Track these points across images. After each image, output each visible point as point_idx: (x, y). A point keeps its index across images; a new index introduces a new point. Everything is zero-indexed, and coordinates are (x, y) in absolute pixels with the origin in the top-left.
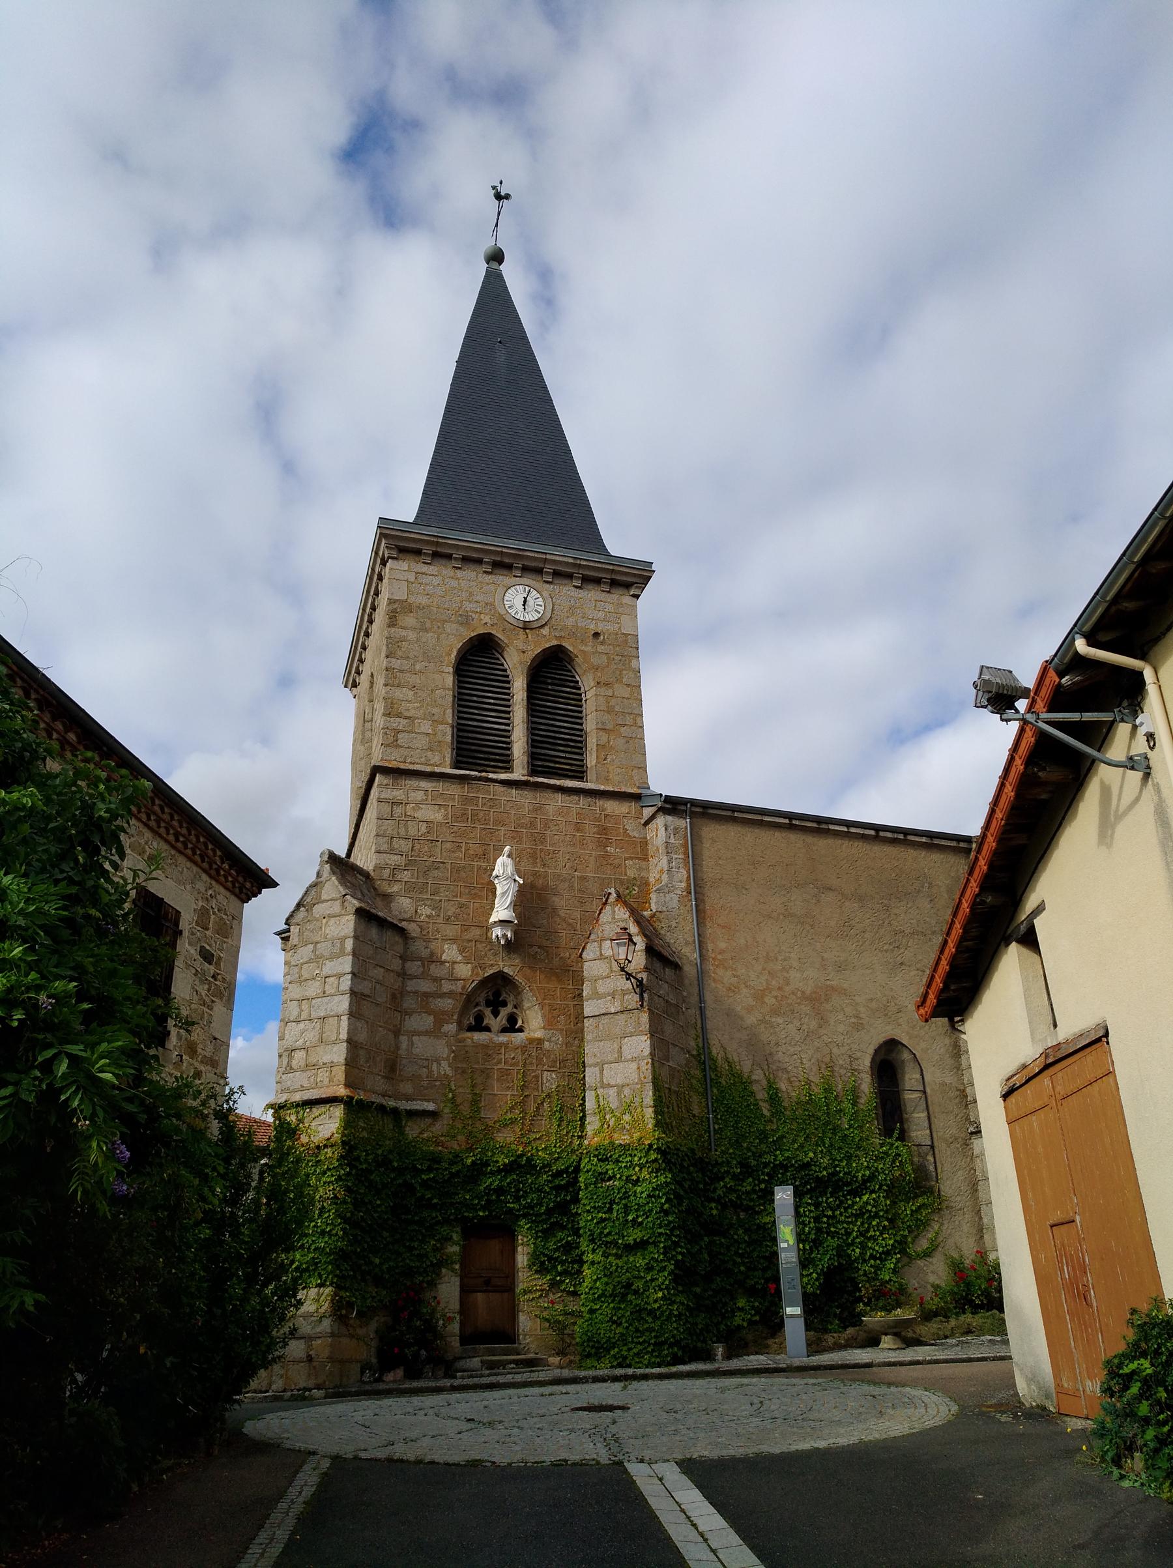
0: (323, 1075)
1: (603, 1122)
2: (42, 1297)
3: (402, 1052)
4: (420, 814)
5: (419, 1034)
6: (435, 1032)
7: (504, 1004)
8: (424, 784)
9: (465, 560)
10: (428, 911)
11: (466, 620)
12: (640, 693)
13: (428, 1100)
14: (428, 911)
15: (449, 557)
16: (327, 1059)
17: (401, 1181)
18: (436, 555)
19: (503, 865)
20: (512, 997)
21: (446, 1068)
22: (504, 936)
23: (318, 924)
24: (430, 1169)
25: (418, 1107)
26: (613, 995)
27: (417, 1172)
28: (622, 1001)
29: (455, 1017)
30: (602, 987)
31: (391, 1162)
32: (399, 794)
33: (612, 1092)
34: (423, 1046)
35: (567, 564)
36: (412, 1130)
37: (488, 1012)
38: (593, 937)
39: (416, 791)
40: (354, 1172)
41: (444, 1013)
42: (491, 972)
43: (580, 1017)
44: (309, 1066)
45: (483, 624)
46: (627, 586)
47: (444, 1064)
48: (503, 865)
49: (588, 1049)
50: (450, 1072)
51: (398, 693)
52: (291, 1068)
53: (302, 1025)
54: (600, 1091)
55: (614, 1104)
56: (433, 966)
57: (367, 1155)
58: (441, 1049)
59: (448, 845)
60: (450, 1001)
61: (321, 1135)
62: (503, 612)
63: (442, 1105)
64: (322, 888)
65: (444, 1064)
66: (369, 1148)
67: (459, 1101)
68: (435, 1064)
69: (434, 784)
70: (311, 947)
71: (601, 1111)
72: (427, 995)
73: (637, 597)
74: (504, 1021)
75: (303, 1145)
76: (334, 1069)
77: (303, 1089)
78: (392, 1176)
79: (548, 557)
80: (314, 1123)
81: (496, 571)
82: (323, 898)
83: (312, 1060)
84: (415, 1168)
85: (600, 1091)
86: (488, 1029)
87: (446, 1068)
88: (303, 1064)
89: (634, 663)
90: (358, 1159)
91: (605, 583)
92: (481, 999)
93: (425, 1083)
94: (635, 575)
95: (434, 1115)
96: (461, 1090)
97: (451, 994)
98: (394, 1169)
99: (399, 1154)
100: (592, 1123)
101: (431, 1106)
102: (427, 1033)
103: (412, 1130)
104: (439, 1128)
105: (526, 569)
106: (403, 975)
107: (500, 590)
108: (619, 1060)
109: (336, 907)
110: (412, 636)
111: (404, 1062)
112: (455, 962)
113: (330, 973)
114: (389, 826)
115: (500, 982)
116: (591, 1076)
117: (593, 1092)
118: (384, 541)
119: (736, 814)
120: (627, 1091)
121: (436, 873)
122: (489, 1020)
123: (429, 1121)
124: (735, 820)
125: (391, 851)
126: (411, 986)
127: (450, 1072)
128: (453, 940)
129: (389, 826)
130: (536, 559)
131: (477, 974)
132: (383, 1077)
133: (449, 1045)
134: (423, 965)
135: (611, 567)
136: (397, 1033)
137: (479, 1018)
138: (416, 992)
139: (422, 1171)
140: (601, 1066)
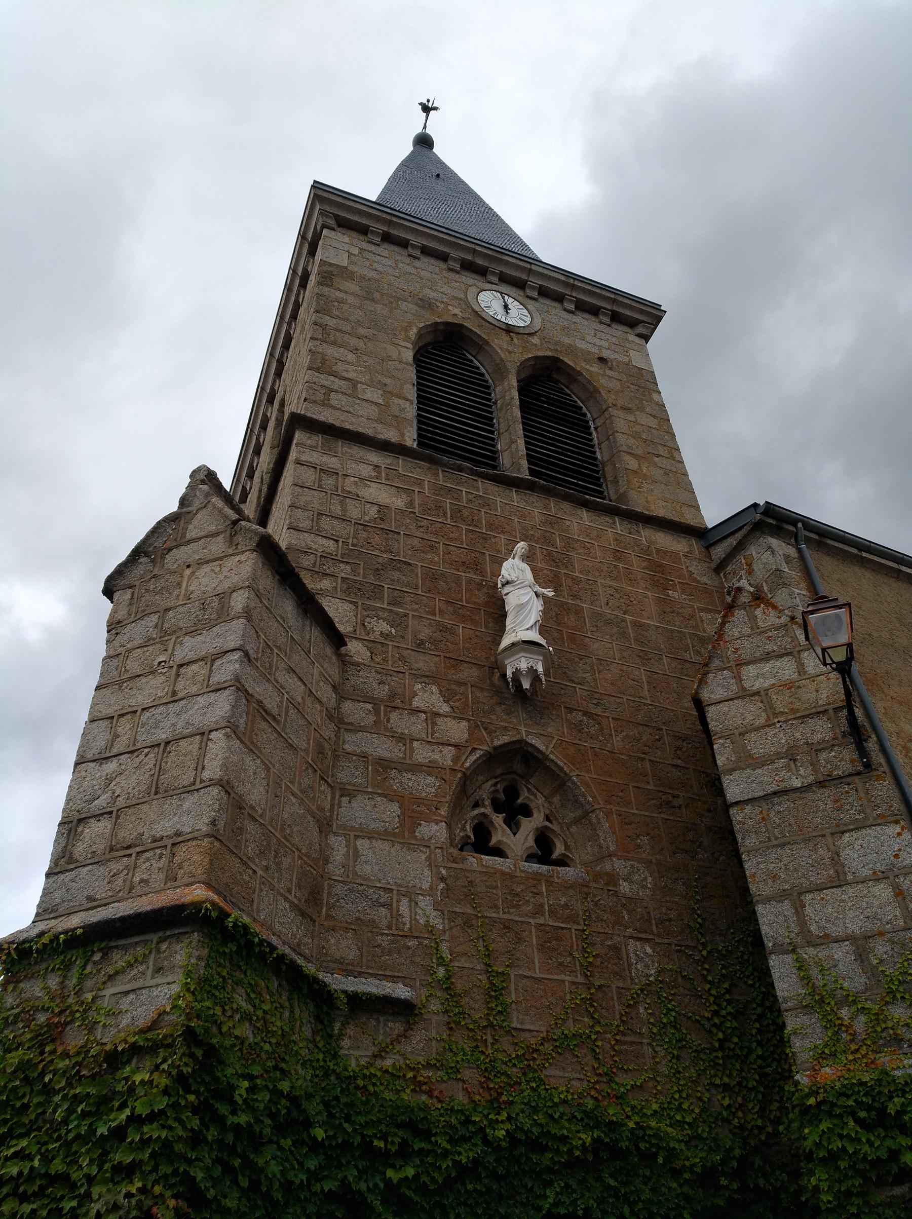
0: (151, 868)
1: (834, 1026)
2: (468, 1182)
3: (335, 870)
4: (365, 493)
5: (371, 835)
6: (404, 834)
7: (527, 812)
8: (374, 457)
9: (426, 251)
10: (384, 627)
11: (426, 304)
12: (670, 427)
13: (394, 979)
14: (384, 627)
15: (404, 244)
16: (164, 827)
17: (329, 1185)
18: (387, 238)
19: (515, 569)
20: (541, 800)
21: (427, 911)
22: (532, 671)
23: (174, 579)
24: (405, 1153)
25: (374, 990)
26: (791, 755)
27: (376, 1159)
28: (814, 764)
29: (443, 812)
30: (758, 745)
31: (308, 1124)
32: (332, 462)
33: (842, 953)
34: (378, 861)
35: (557, 280)
36: (357, 1049)
37: (498, 820)
38: (716, 663)
39: (360, 463)
40: (211, 1134)
41: (419, 801)
42: (506, 739)
43: (721, 807)
44: (118, 849)
45: (455, 313)
46: (632, 324)
47: (424, 902)
48: (515, 569)
49: (750, 866)
50: (437, 922)
51: (331, 351)
52: (71, 860)
53: (111, 766)
54: (807, 954)
55: (854, 980)
56: (394, 716)
57: (252, 1090)
58: (416, 870)
59: (416, 542)
60: (430, 780)
61: (125, 1021)
62: (477, 309)
63: (424, 992)
64: (189, 522)
65: (424, 902)
66: (256, 1070)
67: (459, 985)
68: (405, 902)
69: (389, 461)
70: (154, 618)
71: (819, 1001)
72: (384, 764)
73: (647, 338)
74: (531, 842)
75: (66, 1055)
76: (181, 851)
77: (93, 903)
78: (312, 1164)
79: (534, 267)
80: (109, 991)
81: (463, 273)
82: (188, 536)
83: (126, 834)
84: (367, 1149)
85: (807, 954)
86: (498, 852)
87: (427, 911)
88: (100, 847)
89: (655, 396)
90: (226, 1093)
91: (605, 314)
92: (485, 792)
93: (384, 941)
94: (642, 312)
95: (404, 1010)
96: (463, 962)
97: (431, 768)
98: (315, 1146)
99: (327, 1105)
100: (804, 1034)
101: (401, 992)
102: (386, 835)
103: (357, 1049)
104: (421, 1044)
105: (504, 279)
106: (336, 718)
107: (476, 290)
108: (839, 881)
109: (218, 546)
110: (351, 299)
111: (339, 889)
112: (438, 715)
113: (191, 656)
114: (314, 499)
115: (518, 767)
116: (772, 921)
117: (788, 958)
118: (318, 207)
119: (864, 554)
120: (881, 949)
121: (396, 575)
122: (500, 834)
123: (396, 1027)
124: (863, 563)
125: (316, 531)
126: (352, 743)
127: (437, 922)
128: (429, 678)
129: (314, 499)
130: (518, 267)
131: (481, 740)
132: (294, 907)
133: (431, 863)
134: (377, 712)
135: (612, 296)
136: (325, 826)
137: (482, 832)
138: (364, 756)
139: (386, 1159)
140: (795, 897)
